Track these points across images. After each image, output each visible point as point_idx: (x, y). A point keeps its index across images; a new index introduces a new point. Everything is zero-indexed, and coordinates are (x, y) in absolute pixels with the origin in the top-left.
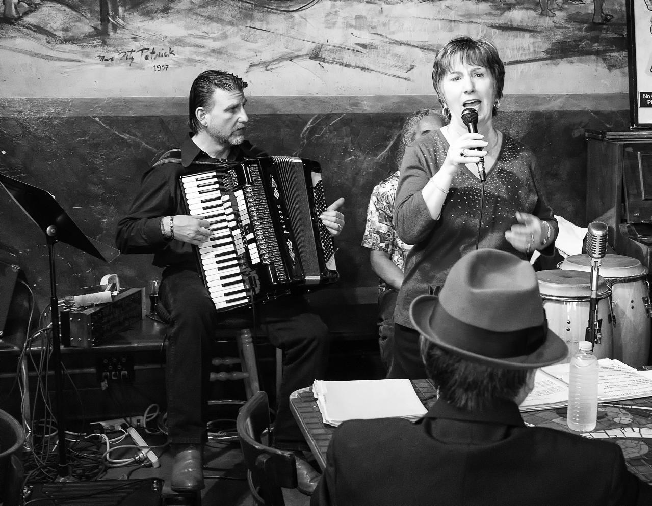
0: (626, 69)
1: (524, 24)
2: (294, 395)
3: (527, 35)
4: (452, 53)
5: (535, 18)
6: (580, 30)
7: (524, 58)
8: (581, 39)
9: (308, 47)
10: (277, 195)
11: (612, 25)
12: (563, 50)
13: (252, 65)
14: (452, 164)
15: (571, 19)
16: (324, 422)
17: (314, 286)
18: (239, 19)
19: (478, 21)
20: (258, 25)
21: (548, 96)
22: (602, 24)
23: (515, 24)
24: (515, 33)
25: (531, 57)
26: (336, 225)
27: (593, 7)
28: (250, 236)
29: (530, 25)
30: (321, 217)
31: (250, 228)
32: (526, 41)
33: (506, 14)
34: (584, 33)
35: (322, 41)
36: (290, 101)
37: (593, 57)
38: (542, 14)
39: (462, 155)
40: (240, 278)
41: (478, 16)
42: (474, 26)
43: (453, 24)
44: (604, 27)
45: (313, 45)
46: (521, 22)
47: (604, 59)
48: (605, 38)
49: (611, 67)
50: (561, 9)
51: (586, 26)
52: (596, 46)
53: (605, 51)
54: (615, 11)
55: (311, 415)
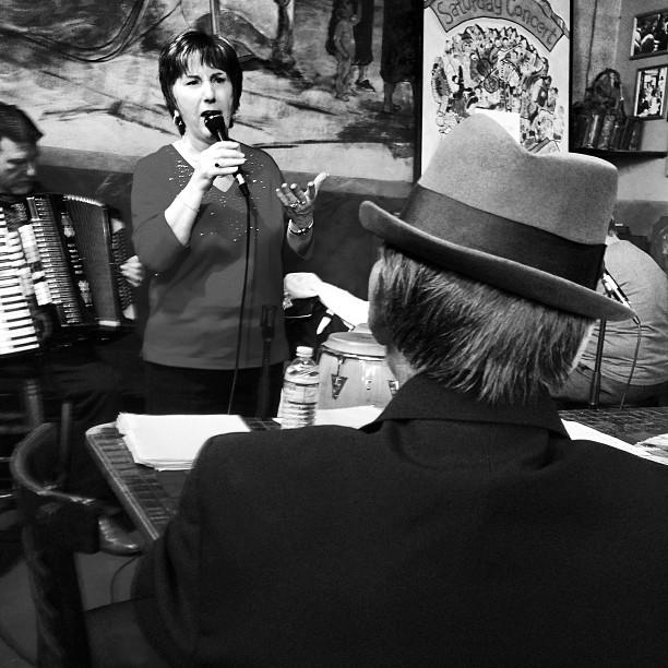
0: (410, 159)
1: (320, 105)
2: (93, 431)
3: (322, 116)
4: (189, 50)
5: (330, 101)
6: (370, 117)
7: (319, 139)
8: (371, 126)
9: (107, 102)
10: (68, 232)
11: (400, 115)
12: (351, 135)
13: (47, 113)
14: (206, 178)
15: (364, 105)
16: (137, 461)
17: (108, 331)
18: (32, 62)
19: (278, 96)
20: (53, 70)
21: (338, 177)
22: (390, 114)
23: (312, 104)
24: (311, 112)
25: (325, 138)
26: (137, 278)
27: (383, 96)
28: (38, 275)
29: (324, 106)
30: (122, 267)
31: (37, 266)
32: (320, 121)
33: (304, 93)
34: (373, 121)
35: (121, 96)
36: (91, 156)
37: (381, 145)
38: (337, 98)
39: (217, 165)
40: (25, 304)
41: (278, 91)
42: (272, 100)
43: (253, 96)
44: (392, 116)
45: (112, 101)
46: (318, 102)
47: (390, 148)
48: (392, 128)
49: (396, 156)
50: (354, 95)
51: (375, 113)
52: (384, 135)
53: (392, 140)
54: (402, 102)
55: (118, 453)
